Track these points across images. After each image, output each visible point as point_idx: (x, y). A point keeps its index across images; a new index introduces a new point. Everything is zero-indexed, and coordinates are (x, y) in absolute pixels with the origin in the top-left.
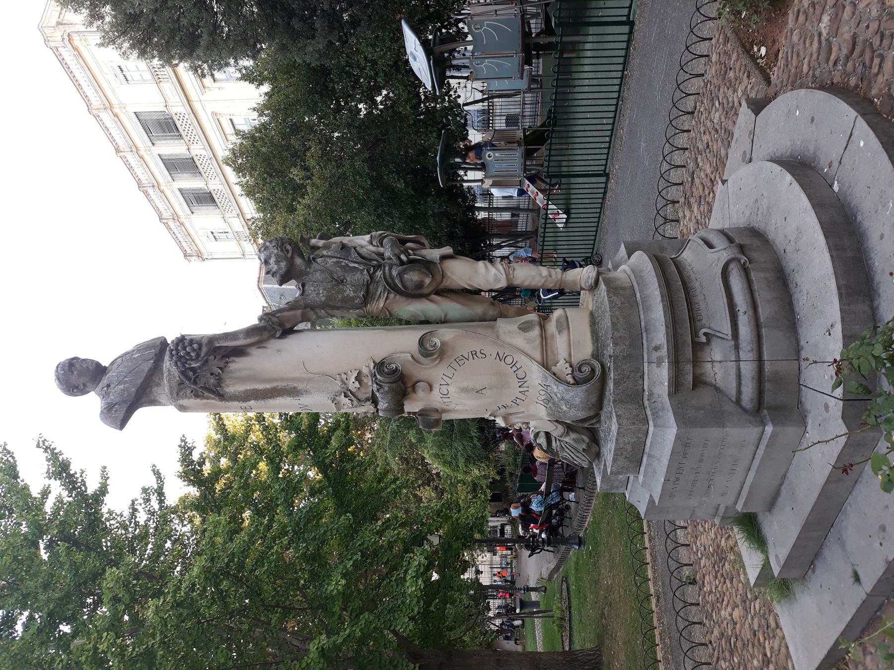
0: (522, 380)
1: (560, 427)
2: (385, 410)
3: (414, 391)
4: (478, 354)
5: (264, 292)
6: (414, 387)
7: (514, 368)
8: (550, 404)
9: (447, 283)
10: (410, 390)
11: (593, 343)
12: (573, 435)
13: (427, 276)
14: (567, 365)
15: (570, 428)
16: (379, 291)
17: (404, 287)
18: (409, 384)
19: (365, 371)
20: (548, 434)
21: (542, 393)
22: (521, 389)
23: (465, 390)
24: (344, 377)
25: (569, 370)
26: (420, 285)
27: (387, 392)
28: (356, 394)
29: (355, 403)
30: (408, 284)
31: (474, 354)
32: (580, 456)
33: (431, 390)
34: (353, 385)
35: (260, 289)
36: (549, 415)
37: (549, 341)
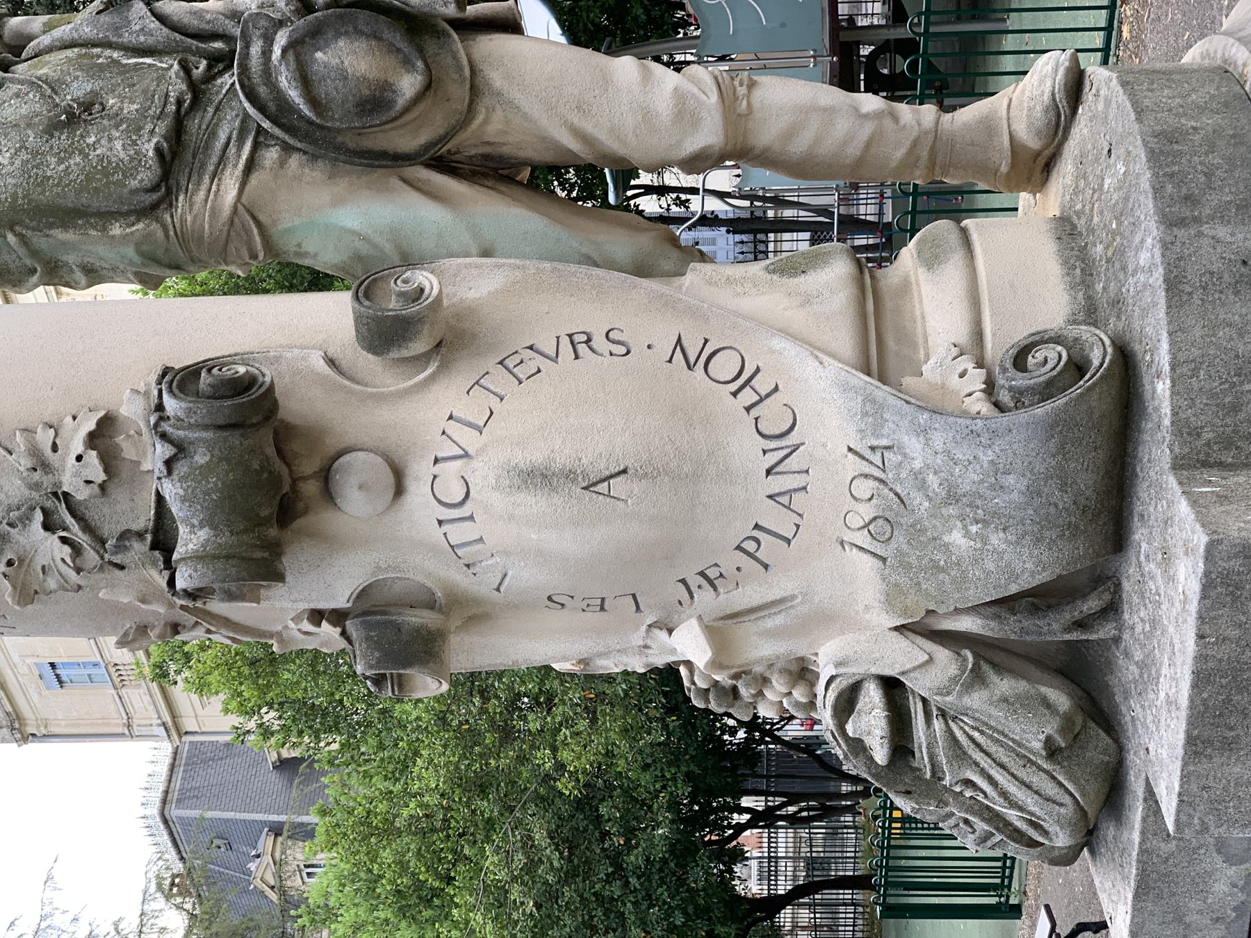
0: (782, 440)
1: (942, 654)
2: (198, 558)
3: (328, 495)
4: (599, 342)
5: (178, 829)
6: (326, 475)
7: (748, 397)
8: (900, 539)
9: (494, 129)
10: (310, 488)
11: (1073, 287)
12: (1004, 685)
13: (407, 64)
14: (967, 363)
15: (986, 655)
16: (223, 137)
17: (313, 101)
18: (308, 467)
19: (133, 410)
20: (892, 687)
21: (865, 488)
22: (777, 484)
23: (539, 478)
24: (45, 438)
25: (976, 380)
26: (375, 103)
27: (206, 470)
28: (92, 515)
29: (91, 557)
30: (328, 89)
31: (580, 342)
32: (1038, 780)
33: (400, 491)
34: (77, 473)
35: (165, 822)
36: (891, 598)
37: (889, 304)
